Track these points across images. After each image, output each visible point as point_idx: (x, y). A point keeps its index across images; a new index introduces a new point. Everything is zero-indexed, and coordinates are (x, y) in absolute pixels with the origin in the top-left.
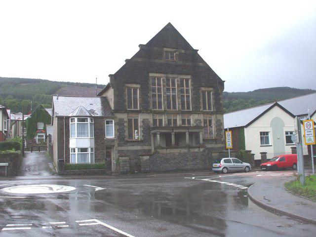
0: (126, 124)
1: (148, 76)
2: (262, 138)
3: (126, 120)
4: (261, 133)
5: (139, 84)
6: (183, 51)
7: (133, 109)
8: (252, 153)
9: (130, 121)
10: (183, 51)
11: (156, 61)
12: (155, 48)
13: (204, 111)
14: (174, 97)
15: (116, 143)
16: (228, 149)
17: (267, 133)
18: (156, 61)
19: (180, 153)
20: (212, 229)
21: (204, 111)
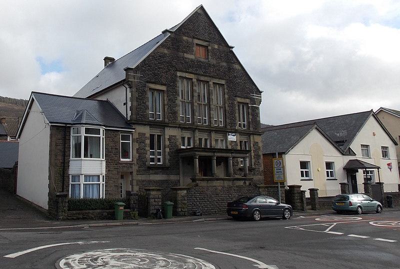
0: (148, 142)
1: (176, 76)
2: (383, 154)
3: (148, 135)
4: (383, 147)
5: (164, 85)
6: (216, 47)
7: (131, 142)
8: (302, 189)
9: (152, 136)
10: (216, 47)
11: (186, 55)
12: (185, 38)
13: (158, 163)
14: (152, 147)
15: (135, 168)
16: (277, 183)
17: (387, 148)
18: (186, 55)
19: (223, 187)
20: (118, 224)
21: (158, 163)
